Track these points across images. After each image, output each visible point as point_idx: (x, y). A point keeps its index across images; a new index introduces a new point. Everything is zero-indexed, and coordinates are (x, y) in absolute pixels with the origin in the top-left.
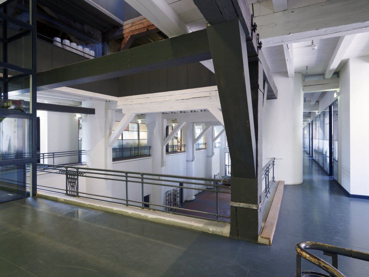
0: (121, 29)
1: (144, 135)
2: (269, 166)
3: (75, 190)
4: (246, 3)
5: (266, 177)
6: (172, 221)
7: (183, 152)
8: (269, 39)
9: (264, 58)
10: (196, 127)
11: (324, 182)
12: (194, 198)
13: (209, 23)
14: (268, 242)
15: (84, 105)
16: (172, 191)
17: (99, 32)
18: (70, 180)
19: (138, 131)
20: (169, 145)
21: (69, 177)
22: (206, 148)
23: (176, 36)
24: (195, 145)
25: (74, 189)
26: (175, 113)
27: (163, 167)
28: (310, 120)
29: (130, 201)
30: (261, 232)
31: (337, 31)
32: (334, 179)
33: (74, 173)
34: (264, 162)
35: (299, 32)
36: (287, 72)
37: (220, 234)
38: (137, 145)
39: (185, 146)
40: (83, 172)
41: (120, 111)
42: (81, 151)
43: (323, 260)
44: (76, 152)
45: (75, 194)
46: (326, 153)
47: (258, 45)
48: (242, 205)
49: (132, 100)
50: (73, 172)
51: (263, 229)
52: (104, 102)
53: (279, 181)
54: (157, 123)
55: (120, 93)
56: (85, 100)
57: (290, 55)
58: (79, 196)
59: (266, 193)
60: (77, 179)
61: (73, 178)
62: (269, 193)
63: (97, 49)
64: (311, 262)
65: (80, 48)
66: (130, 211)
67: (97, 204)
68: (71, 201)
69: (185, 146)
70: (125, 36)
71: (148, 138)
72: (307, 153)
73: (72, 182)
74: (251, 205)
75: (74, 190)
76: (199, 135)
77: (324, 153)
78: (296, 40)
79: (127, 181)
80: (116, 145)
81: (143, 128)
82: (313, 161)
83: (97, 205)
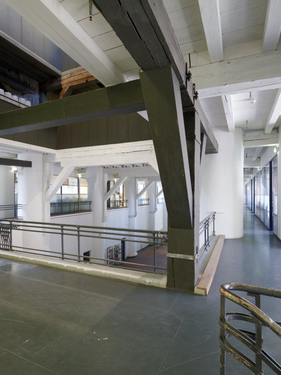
0: (58, 80)
1: (84, 190)
2: (209, 219)
3: (8, 244)
4: (179, 51)
5: (205, 230)
6: (109, 274)
7: (125, 207)
8: (206, 90)
9: (202, 110)
10: (139, 182)
11: (264, 236)
12: (136, 254)
13: (142, 69)
14: (204, 293)
15: (20, 158)
16: (114, 247)
17: (36, 81)
18: (3, 234)
19: (78, 186)
20: (111, 200)
21: (2, 230)
22: (148, 204)
23: (113, 85)
24: (137, 201)
25: (7, 243)
26: (116, 167)
27: (104, 223)
28: (252, 176)
29: (65, 254)
30: (197, 283)
31: (272, 83)
32: (274, 233)
33: (7, 226)
34: (201, 215)
35: (235, 83)
36: (227, 127)
37: (157, 286)
38: (77, 201)
39: (127, 201)
40: (17, 225)
41: (58, 165)
42: (17, 205)
43: (244, 299)
44: (12, 206)
45: (8, 248)
46: (267, 208)
47: (194, 95)
48: (179, 256)
49: (71, 153)
50: (8, 225)
51: (199, 280)
52: (41, 155)
53: (220, 236)
54: (97, 178)
55: (59, 146)
56: (21, 152)
57: (230, 108)
58: (13, 250)
59: (206, 246)
60: (11, 232)
61: (6, 232)
62: (208, 246)
63: (34, 99)
64: (233, 301)
65: (15, 97)
66: (65, 264)
67: (31, 257)
68: (4, 255)
69: (127, 201)
70: (63, 87)
71: (88, 193)
72: (249, 209)
73: (5, 236)
74: (188, 256)
75: (7, 244)
76: (141, 190)
77: (265, 209)
78: (233, 92)
79: (62, 234)
80: (54, 199)
81: (83, 182)
82: (255, 216)
83: (31, 258)
